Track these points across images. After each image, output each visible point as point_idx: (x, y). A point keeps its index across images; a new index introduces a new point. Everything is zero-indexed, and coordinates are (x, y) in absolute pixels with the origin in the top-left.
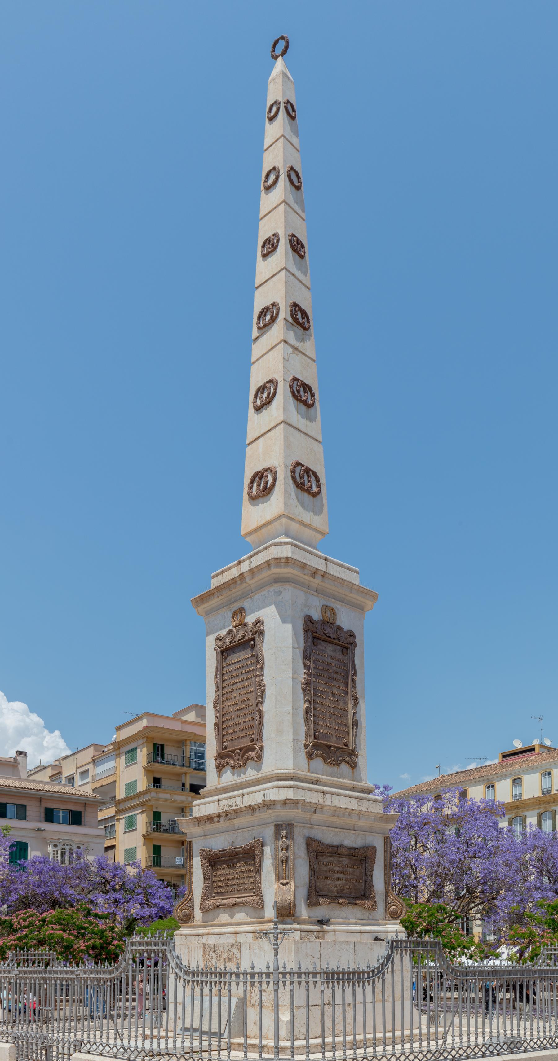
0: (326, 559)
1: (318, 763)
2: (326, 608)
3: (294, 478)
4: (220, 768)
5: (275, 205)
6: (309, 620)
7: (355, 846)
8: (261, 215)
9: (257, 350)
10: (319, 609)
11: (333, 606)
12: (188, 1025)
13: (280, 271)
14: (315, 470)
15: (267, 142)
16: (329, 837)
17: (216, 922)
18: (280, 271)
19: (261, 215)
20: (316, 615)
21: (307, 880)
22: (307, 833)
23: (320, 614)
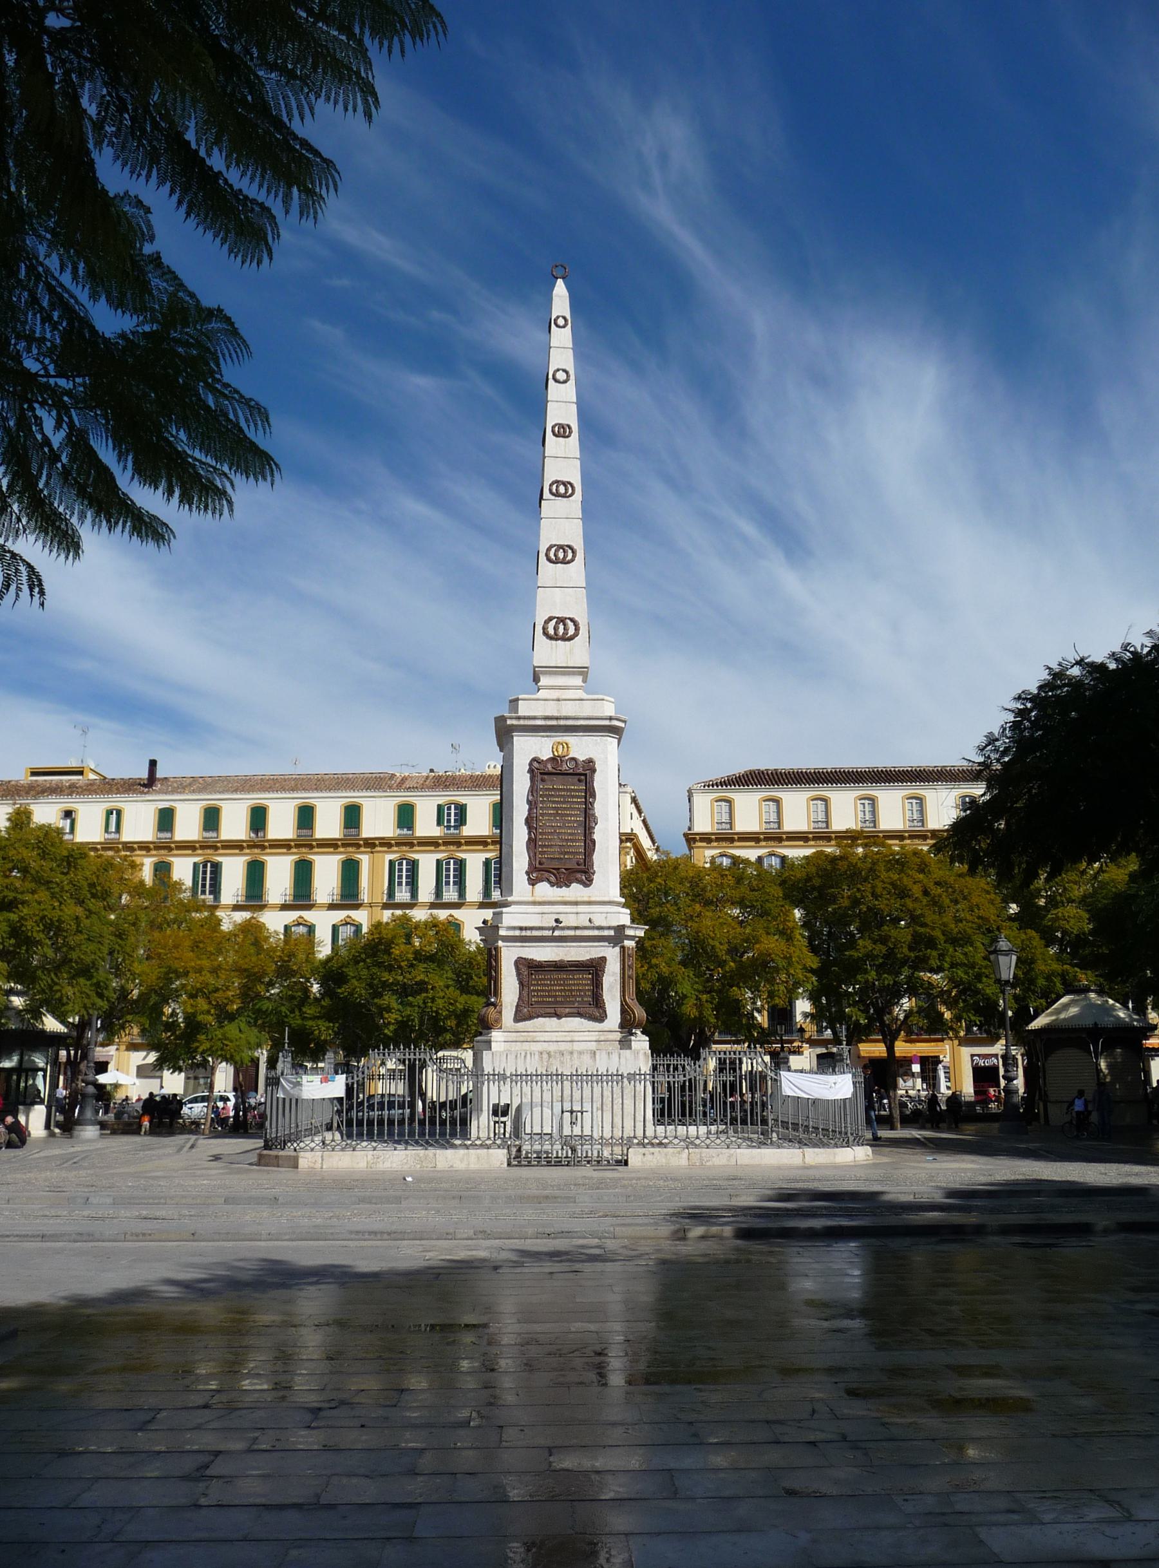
4: (533, 882)
12: (537, 1130)
20: (546, 755)
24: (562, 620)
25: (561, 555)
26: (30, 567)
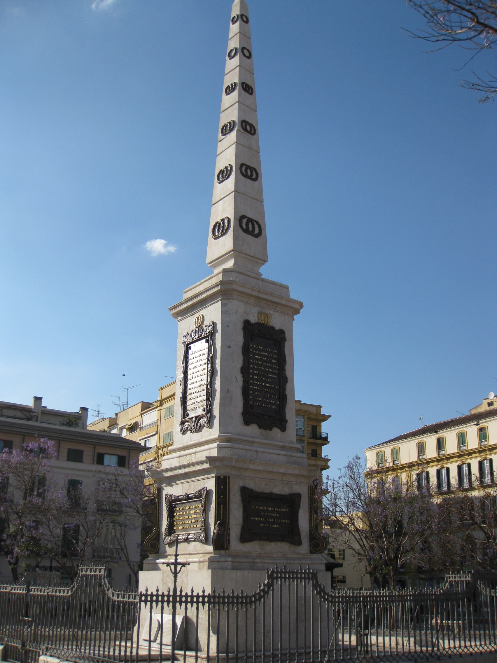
0: (256, 451)
1: (253, 429)
2: (260, 313)
3: (242, 173)
5: (234, 68)
6: (247, 324)
7: (283, 493)
8: (226, 72)
9: (221, 147)
10: (256, 315)
11: (268, 312)
13: (236, 68)
14: (257, 220)
15: (231, 35)
16: (259, 485)
17: (195, 620)
18: (236, 68)
19: (226, 72)
20: (253, 319)
21: (241, 520)
22: (241, 483)
23: (256, 318)
24: (250, 220)
25: (249, 173)
26: (255, 221)
